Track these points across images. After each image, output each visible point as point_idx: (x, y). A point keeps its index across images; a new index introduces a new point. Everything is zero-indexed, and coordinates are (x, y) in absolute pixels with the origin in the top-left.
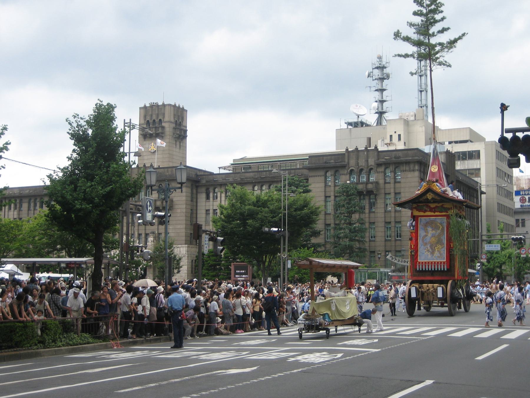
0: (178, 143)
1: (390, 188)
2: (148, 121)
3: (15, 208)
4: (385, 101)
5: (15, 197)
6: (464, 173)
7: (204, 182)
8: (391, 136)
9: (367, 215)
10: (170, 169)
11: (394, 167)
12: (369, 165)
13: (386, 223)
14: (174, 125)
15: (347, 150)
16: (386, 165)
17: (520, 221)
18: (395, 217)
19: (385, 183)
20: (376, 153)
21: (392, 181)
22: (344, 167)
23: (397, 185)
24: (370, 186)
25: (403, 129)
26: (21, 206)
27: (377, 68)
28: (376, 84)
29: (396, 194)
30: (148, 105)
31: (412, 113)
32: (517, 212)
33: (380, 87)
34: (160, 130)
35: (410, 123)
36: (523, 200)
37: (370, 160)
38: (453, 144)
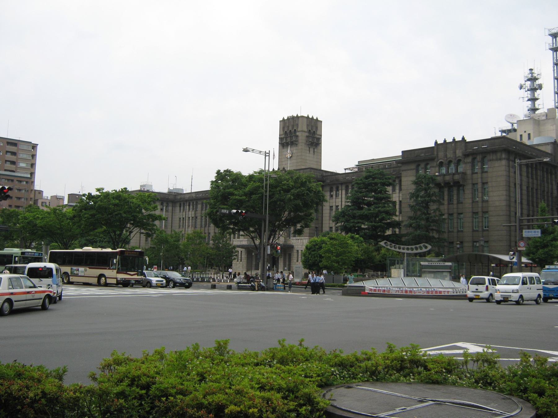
0: (312, 150)
1: (478, 178)
2: (286, 132)
3: (193, 209)
7: (328, 181)
8: (521, 136)
9: (455, 206)
12: (457, 156)
13: (474, 213)
14: (307, 134)
15: (436, 143)
20: (463, 144)
21: (479, 171)
22: (433, 159)
24: (457, 177)
26: (196, 208)
27: (529, 80)
28: (528, 95)
29: (483, 184)
30: (286, 118)
34: (294, 139)
37: (457, 151)
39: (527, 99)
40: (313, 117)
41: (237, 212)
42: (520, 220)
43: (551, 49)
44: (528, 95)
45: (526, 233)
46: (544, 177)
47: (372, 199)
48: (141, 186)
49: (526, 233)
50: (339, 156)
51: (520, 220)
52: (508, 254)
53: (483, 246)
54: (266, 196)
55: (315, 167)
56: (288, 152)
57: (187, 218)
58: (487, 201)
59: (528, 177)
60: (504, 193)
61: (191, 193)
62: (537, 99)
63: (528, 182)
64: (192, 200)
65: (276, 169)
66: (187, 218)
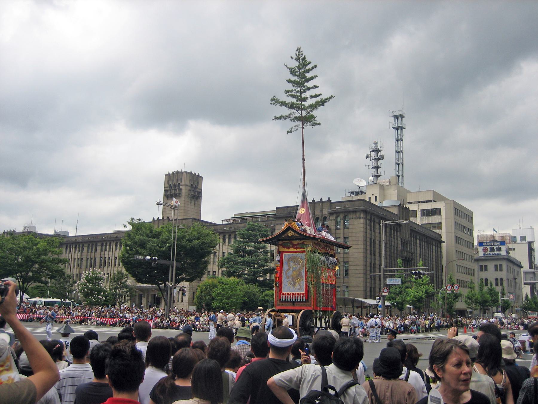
3: (79, 251)
4: (380, 176)
5: (79, 243)
6: (426, 226)
8: (370, 198)
10: (184, 221)
11: (343, 215)
14: (190, 188)
16: (337, 214)
17: (484, 267)
18: (344, 258)
19: (336, 229)
21: (342, 227)
23: (346, 231)
25: (379, 192)
27: (373, 151)
28: (373, 163)
30: (171, 173)
31: (388, 180)
32: (478, 260)
33: (376, 166)
34: (178, 192)
35: (386, 188)
36: (485, 250)
38: (420, 204)
39: (372, 167)
40: (195, 173)
41: (151, 258)
42: (384, 270)
43: (394, 128)
44: (373, 163)
45: (389, 281)
46: (391, 234)
47: (252, 248)
48: (24, 227)
49: (389, 281)
50: (216, 208)
51: (384, 270)
52: (375, 299)
53: (344, 291)
54: (174, 246)
55: (195, 217)
56: (174, 201)
57: (73, 260)
58: (348, 253)
59: (371, 230)
60: (362, 246)
61: (76, 236)
62: (380, 167)
63: (371, 235)
64: (78, 243)
65: (161, 218)
66: (73, 260)
